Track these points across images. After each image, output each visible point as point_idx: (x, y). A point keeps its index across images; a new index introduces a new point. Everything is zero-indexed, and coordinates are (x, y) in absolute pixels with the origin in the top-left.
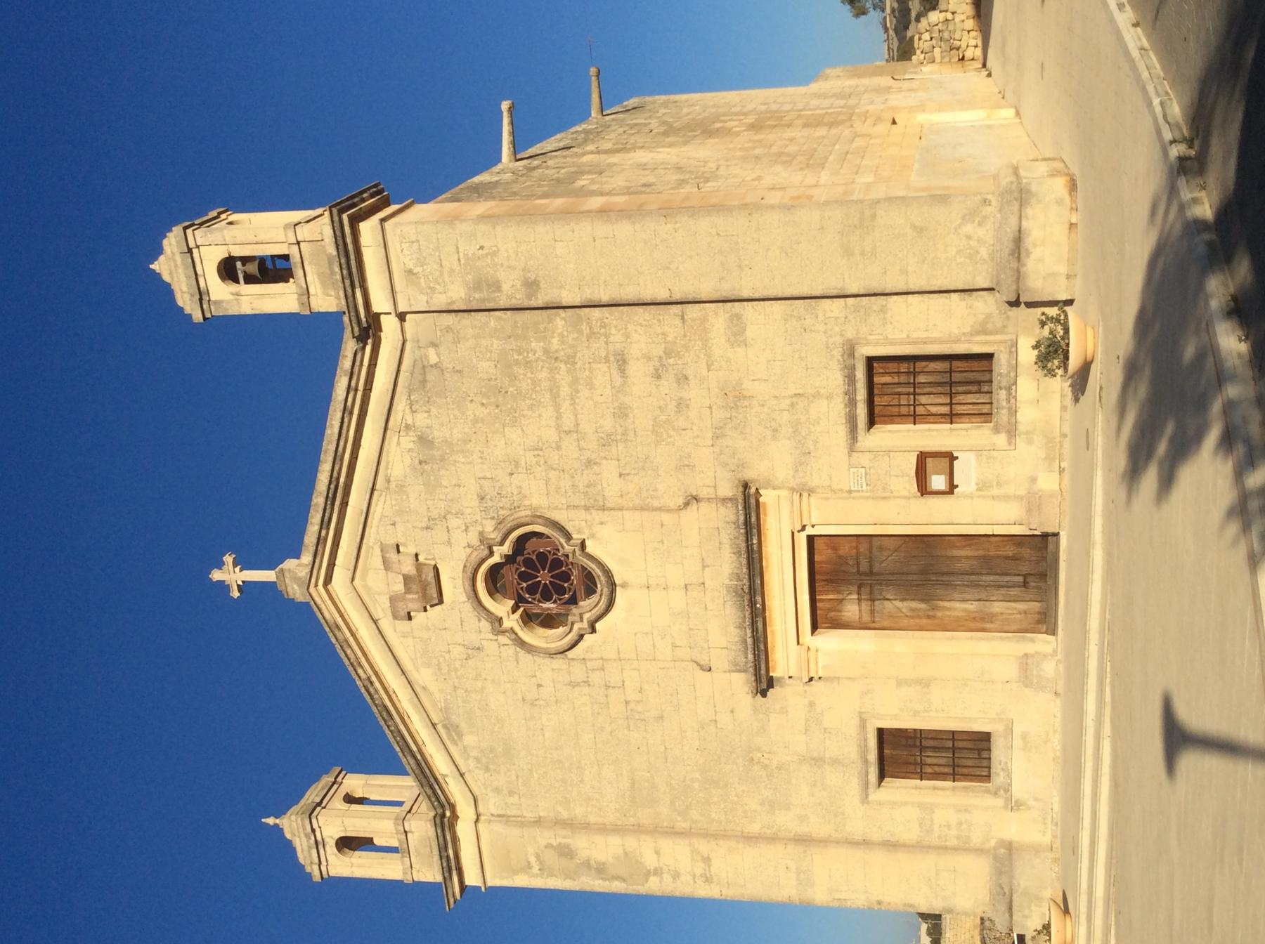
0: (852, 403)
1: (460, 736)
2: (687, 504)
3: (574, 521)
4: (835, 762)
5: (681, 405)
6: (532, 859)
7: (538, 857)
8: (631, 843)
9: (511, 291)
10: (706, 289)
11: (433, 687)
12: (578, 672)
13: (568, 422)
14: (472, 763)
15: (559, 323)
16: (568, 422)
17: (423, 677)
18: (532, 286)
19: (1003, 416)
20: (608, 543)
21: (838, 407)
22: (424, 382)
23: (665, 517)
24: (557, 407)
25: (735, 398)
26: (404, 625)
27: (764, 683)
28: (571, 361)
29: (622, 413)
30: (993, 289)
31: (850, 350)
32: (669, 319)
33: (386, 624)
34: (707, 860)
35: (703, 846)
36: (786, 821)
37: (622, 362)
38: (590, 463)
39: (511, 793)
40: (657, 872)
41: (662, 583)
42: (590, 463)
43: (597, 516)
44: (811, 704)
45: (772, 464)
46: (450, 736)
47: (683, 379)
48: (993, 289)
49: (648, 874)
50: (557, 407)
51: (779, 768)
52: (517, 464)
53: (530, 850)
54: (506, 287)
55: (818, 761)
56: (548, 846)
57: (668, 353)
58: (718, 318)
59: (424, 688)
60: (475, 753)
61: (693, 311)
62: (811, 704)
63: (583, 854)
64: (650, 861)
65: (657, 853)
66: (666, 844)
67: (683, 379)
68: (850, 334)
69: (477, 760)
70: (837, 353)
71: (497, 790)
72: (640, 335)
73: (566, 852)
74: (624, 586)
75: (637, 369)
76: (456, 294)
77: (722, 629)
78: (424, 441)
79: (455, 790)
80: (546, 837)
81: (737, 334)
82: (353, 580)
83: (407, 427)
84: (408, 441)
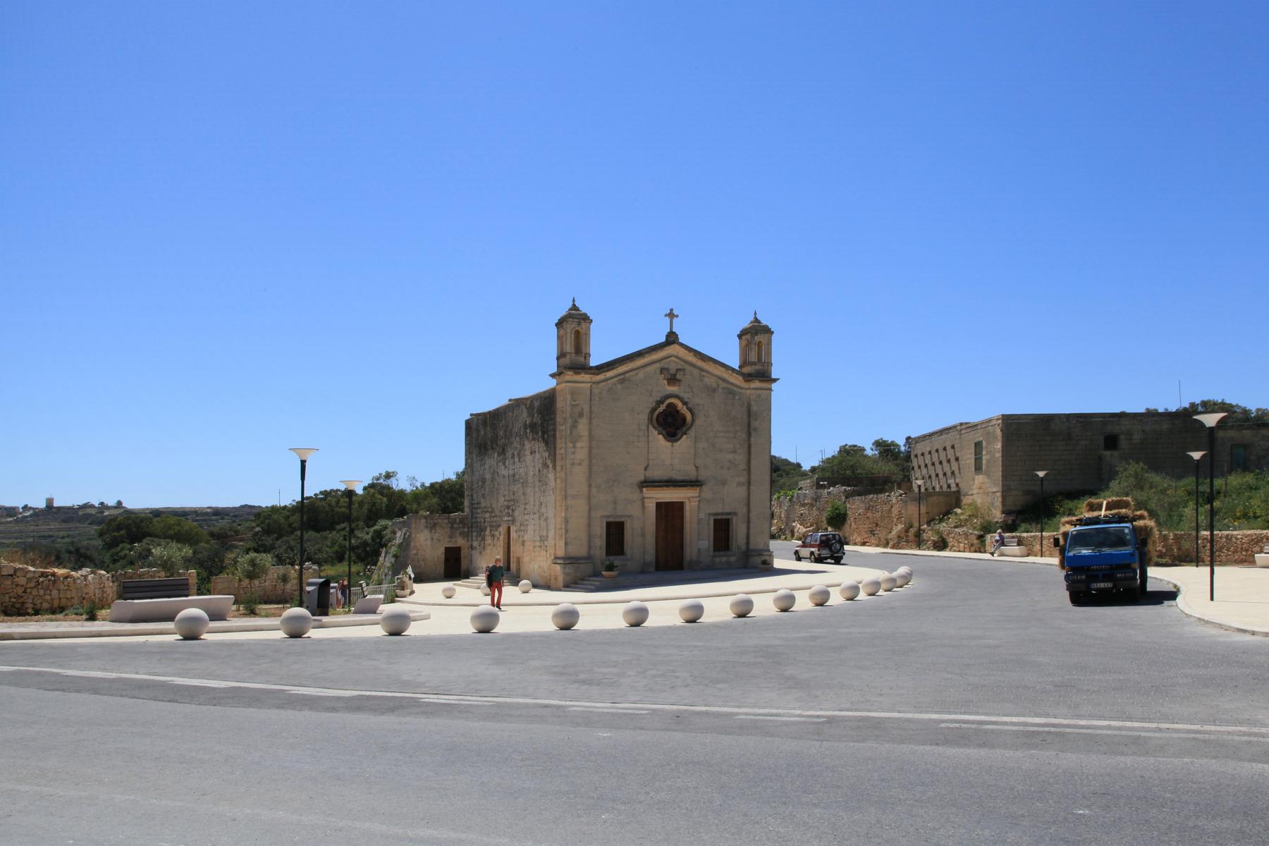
3: (692, 432)
5: (722, 468)
8: (586, 439)
9: (755, 424)
10: (753, 477)
12: (644, 427)
17: (641, 374)
18: (755, 430)
20: (684, 442)
21: (720, 511)
25: (724, 483)
27: (1212, 599)
29: (721, 450)
30: (303, 463)
31: (735, 514)
32: (743, 466)
33: (658, 365)
35: (586, 463)
36: (594, 490)
37: (734, 452)
40: (574, 447)
41: (670, 455)
45: (707, 492)
48: (303, 463)
49: (574, 443)
55: (615, 502)
58: (743, 479)
61: (745, 473)
66: (585, 451)
72: (740, 458)
73: (581, 415)
75: (731, 456)
76: (754, 408)
77: (657, 474)
78: (714, 390)
79: (601, 377)
80: (586, 408)
81: (739, 484)
84: (714, 385)
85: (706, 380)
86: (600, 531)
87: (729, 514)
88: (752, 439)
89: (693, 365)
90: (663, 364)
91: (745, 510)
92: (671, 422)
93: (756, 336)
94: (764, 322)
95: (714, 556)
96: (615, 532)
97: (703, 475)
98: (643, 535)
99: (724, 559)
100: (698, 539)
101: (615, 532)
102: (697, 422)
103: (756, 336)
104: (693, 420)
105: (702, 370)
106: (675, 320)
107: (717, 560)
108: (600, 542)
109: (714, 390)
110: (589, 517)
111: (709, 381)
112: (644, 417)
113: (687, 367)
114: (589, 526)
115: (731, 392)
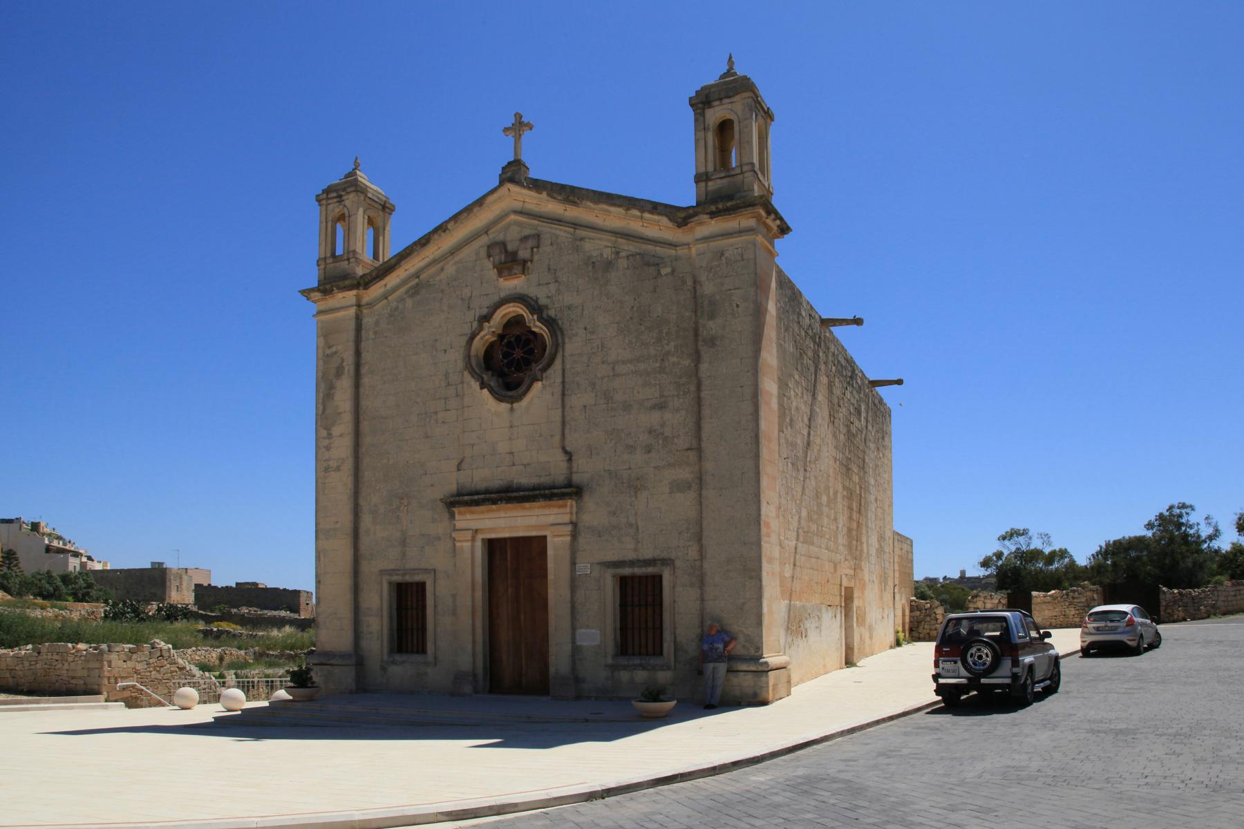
0: (632, 563)
1: (412, 296)
2: (566, 452)
3: (555, 371)
4: (404, 554)
5: (631, 449)
6: (334, 349)
7: (336, 353)
11: (443, 276)
13: (621, 369)
14: (394, 304)
15: (687, 362)
16: (621, 369)
17: (450, 269)
18: (712, 342)
19: (623, 661)
20: (539, 396)
21: (631, 556)
22: (648, 264)
23: (557, 438)
24: (630, 361)
25: (635, 485)
26: (483, 252)
28: (662, 370)
29: (627, 407)
31: (666, 562)
34: (338, 469)
37: (661, 407)
38: (593, 385)
39: (375, 333)
40: (330, 436)
41: (509, 432)
42: (593, 385)
43: (558, 389)
44: (439, 539)
45: (594, 513)
46: (411, 288)
47: (648, 449)
50: (630, 361)
51: (398, 517)
52: (592, 333)
53: (339, 348)
54: (711, 323)
55: (404, 543)
56: (343, 360)
57: (666, 439)
59: (442, 269)
60: (401, 306)
62: (439, 539)
63: (338, 384)
64: (336, 431)
65: (341, 435)
67: (648, 449)
68: (678, 563)
69: (397, 308)
70: (665, 555)
71: (377, 323)
72: (676, 420)
73: (339, 372)
74: (512, 410)
75: (655, 418)
76: (708, 288)
77: (483, 476)
78: (609, 265)
81: (678, 487)
82: (516, 212)
83: (618, 253)
84: (608, 253)
85: (588, 246)
86: (377, 599)
87: (652, 562)
88: (704, 367)
89: (558, 221)
90: (495, 235)
91: (693, 553)
92: (512, 360)
93: (727, 113)
94: (740, 71)
95: (614, 668)
96: (409, 600)
97: (584, 469)
98: (454, 613)
99: (641, 676)
100: (581, 624)
101: (409, 600)
102: (573, 346)
103: (727, 113)
104: (556, 346)
105: (575, 225)
106: (527, 135)
107: (624, 676)
108: (378, 626)
109: (609, 265)
110: (356, 572)
111: (597, 246)
112: (456, 357)
113: (545, 228)
114: (356, 589)
115: (648, 262)
